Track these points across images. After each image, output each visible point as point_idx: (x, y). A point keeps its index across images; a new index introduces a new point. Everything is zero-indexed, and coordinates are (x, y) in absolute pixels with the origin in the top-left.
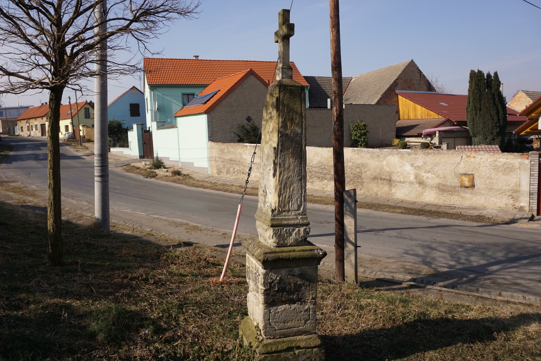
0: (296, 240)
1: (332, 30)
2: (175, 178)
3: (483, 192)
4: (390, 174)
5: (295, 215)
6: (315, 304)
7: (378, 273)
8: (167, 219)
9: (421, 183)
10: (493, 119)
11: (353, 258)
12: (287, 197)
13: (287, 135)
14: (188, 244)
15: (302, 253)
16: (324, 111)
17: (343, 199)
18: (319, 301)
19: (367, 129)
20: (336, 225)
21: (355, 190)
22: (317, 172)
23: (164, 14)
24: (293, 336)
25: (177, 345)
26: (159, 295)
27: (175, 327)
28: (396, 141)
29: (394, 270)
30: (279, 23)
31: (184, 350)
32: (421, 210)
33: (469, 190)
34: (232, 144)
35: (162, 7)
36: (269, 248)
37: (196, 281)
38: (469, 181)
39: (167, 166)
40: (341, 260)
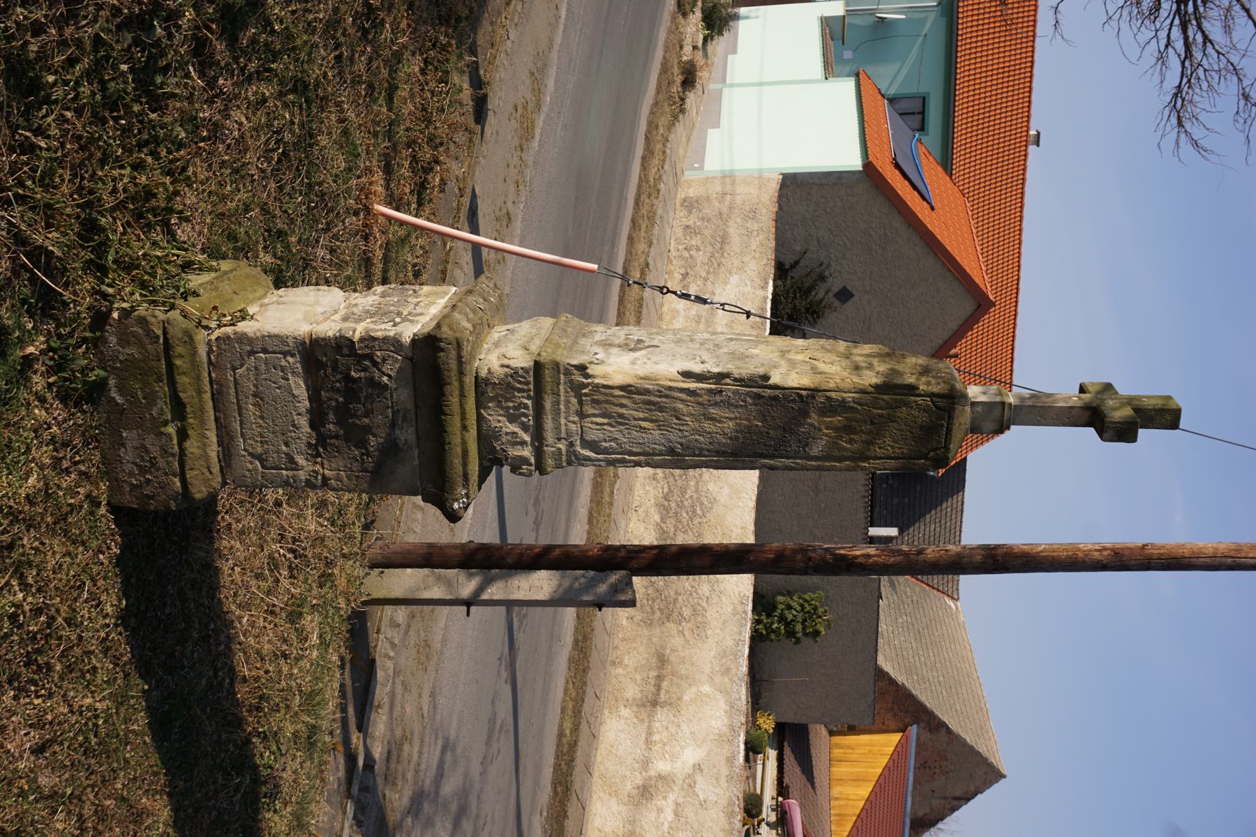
0: (496, 434)
1: (1105, 549)
2: (676, 70)
4: (674, 705)
5: (569, 434)
6: (310, 484)
7: (390, 664)
8: (556, 47)
9: (645, 792)
11: (436, 593)
12: (623, 411)
13: (805, 414)
14: (480, 110)
15: (459, 450)
16: (862, 516)
17: (608, 571)
18: (313, 497)
19: (807, 642)
20: (531, 547)
21: (632, 603)
22: (683, 492)
23: (1179, 45)
24: (216, 420)
25: (188, 75)
26: (334, 23)
27: (242, 70)
28: (767, 724)
29: (398, 709)
30: (1138, 398)
31: (173, 95)
32: (568, 789)
34: (773, 244)
35: (1199, 38)
36: (473, 356)
37: (376, 135)
39: (710, 48)
40: (431, 558)
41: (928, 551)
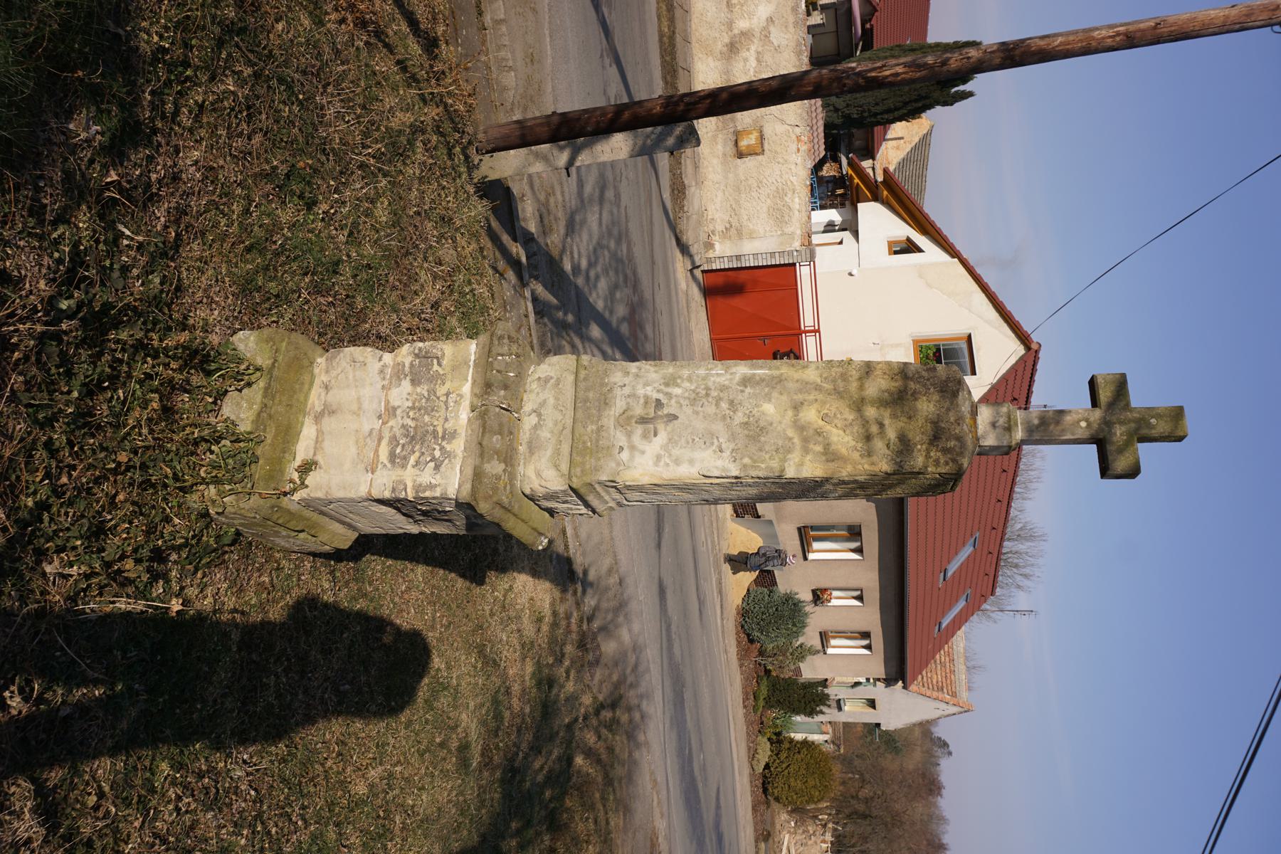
3: (731, 175)
9: (733, 48)
10: (877, 104)
33: (730, 149)
38: (748, 146)
41: (952, 61)
